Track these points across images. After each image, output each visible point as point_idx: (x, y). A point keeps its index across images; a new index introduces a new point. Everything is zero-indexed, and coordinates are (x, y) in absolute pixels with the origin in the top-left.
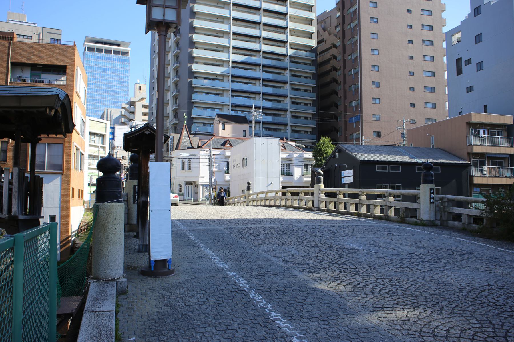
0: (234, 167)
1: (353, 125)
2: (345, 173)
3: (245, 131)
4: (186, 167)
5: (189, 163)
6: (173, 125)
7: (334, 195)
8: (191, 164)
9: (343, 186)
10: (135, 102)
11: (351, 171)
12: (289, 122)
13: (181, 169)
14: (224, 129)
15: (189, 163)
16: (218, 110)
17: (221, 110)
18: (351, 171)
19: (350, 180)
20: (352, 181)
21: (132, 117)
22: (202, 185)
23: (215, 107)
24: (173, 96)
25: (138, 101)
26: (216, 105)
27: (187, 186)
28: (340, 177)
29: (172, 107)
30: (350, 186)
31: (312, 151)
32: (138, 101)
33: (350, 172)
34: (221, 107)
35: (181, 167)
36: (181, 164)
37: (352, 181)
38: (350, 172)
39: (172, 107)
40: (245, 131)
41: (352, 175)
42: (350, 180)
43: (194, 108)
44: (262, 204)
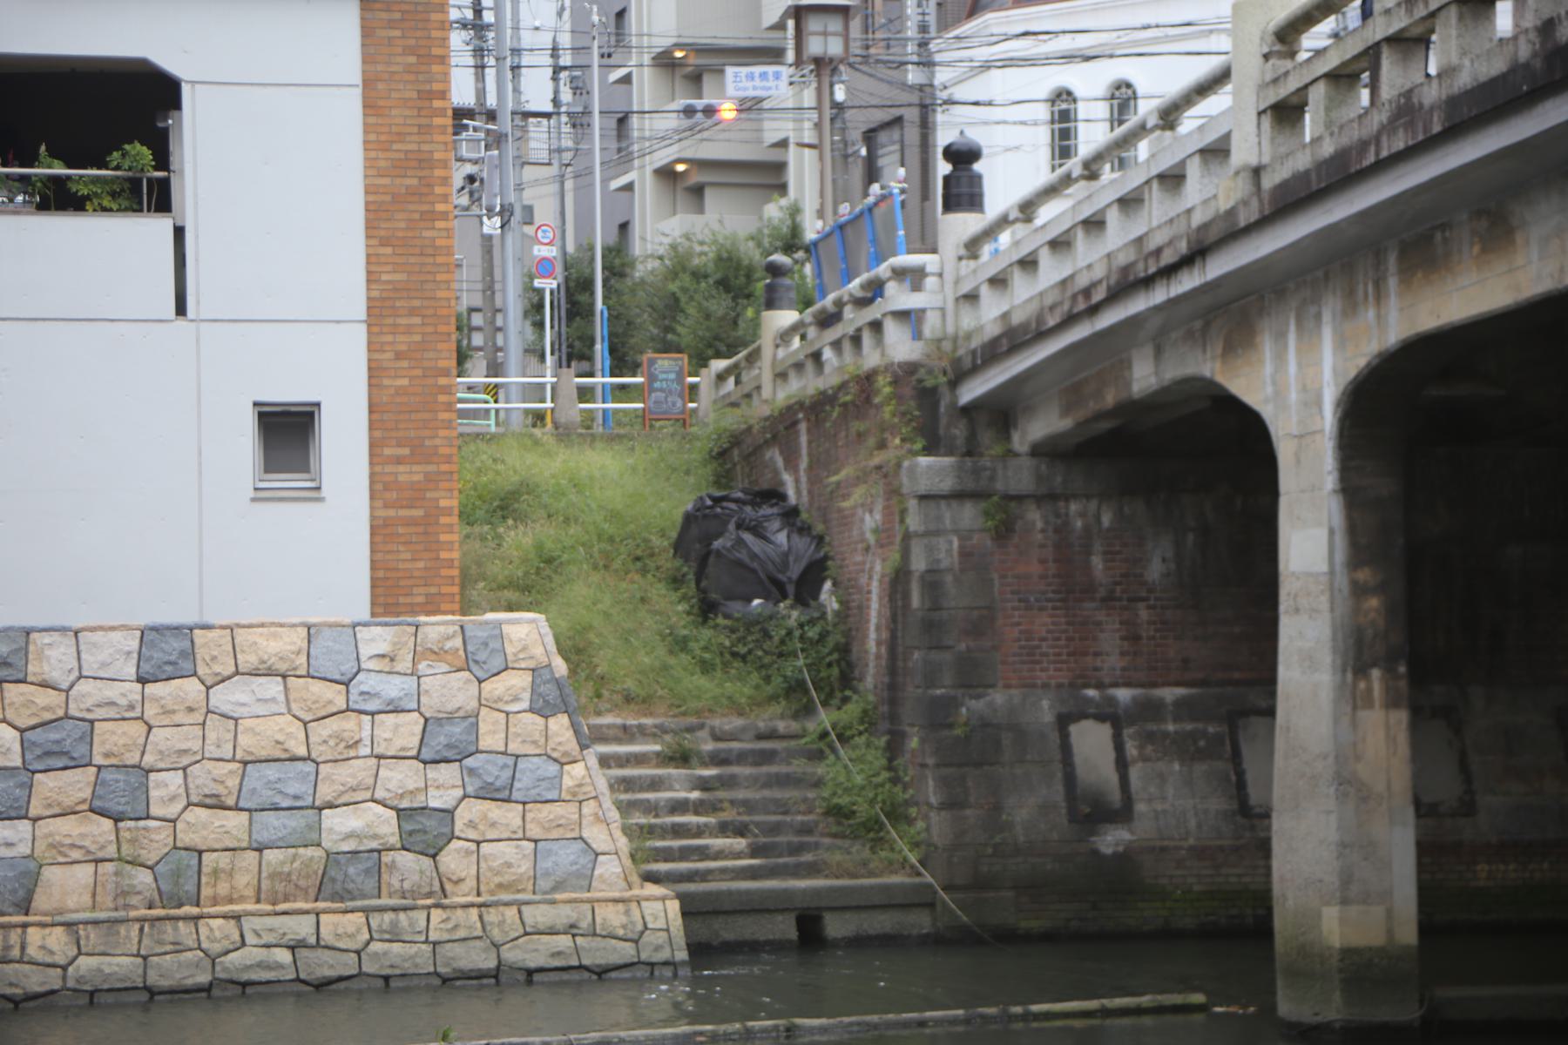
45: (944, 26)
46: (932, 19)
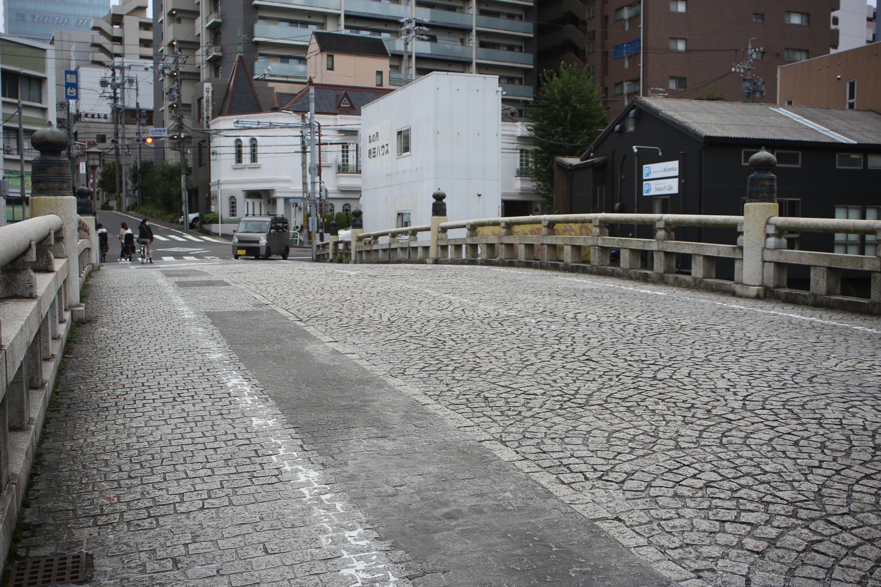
0: (372, 153)
1: (623, 64)
2: (652, 170)
3: (380, 73)
4: (246, 158)
5: (239, 159)
6: (209, 61)
7: (822, 240)
8: (259, 150)
9: (647, 204)
10: (122, 16)
11: (675, 164)
12: (474, 57)
13: (234, 161)
14: (332, 69)
15: (239, 159)
16: (315, 27)
17: (322, 25)
18: (675, 164)
19: (672, 187)
20: (675, 190)
21: (117, 49)
22: (286, 200)
23: (306, 19)
24: (209, 28)
25: (129, 14)
26: (310, 14)
27: (250, 201)
28: (641, 181)
29: (207, 20)
30: (667, 203)
31: (535, 118)
32: (129, 14)
33: (673, 167)
34: (321, 21)
35: (234, 156)
36: (233, 150)
37: (675, 190)
38: (673, 167)
39: (207, 54)
40: (380, 73)
41: (676, 173)
42: (672, 187)
43: (260, 21)
44: (15, 147)
45: (214, 117)
46: (210, 115)
